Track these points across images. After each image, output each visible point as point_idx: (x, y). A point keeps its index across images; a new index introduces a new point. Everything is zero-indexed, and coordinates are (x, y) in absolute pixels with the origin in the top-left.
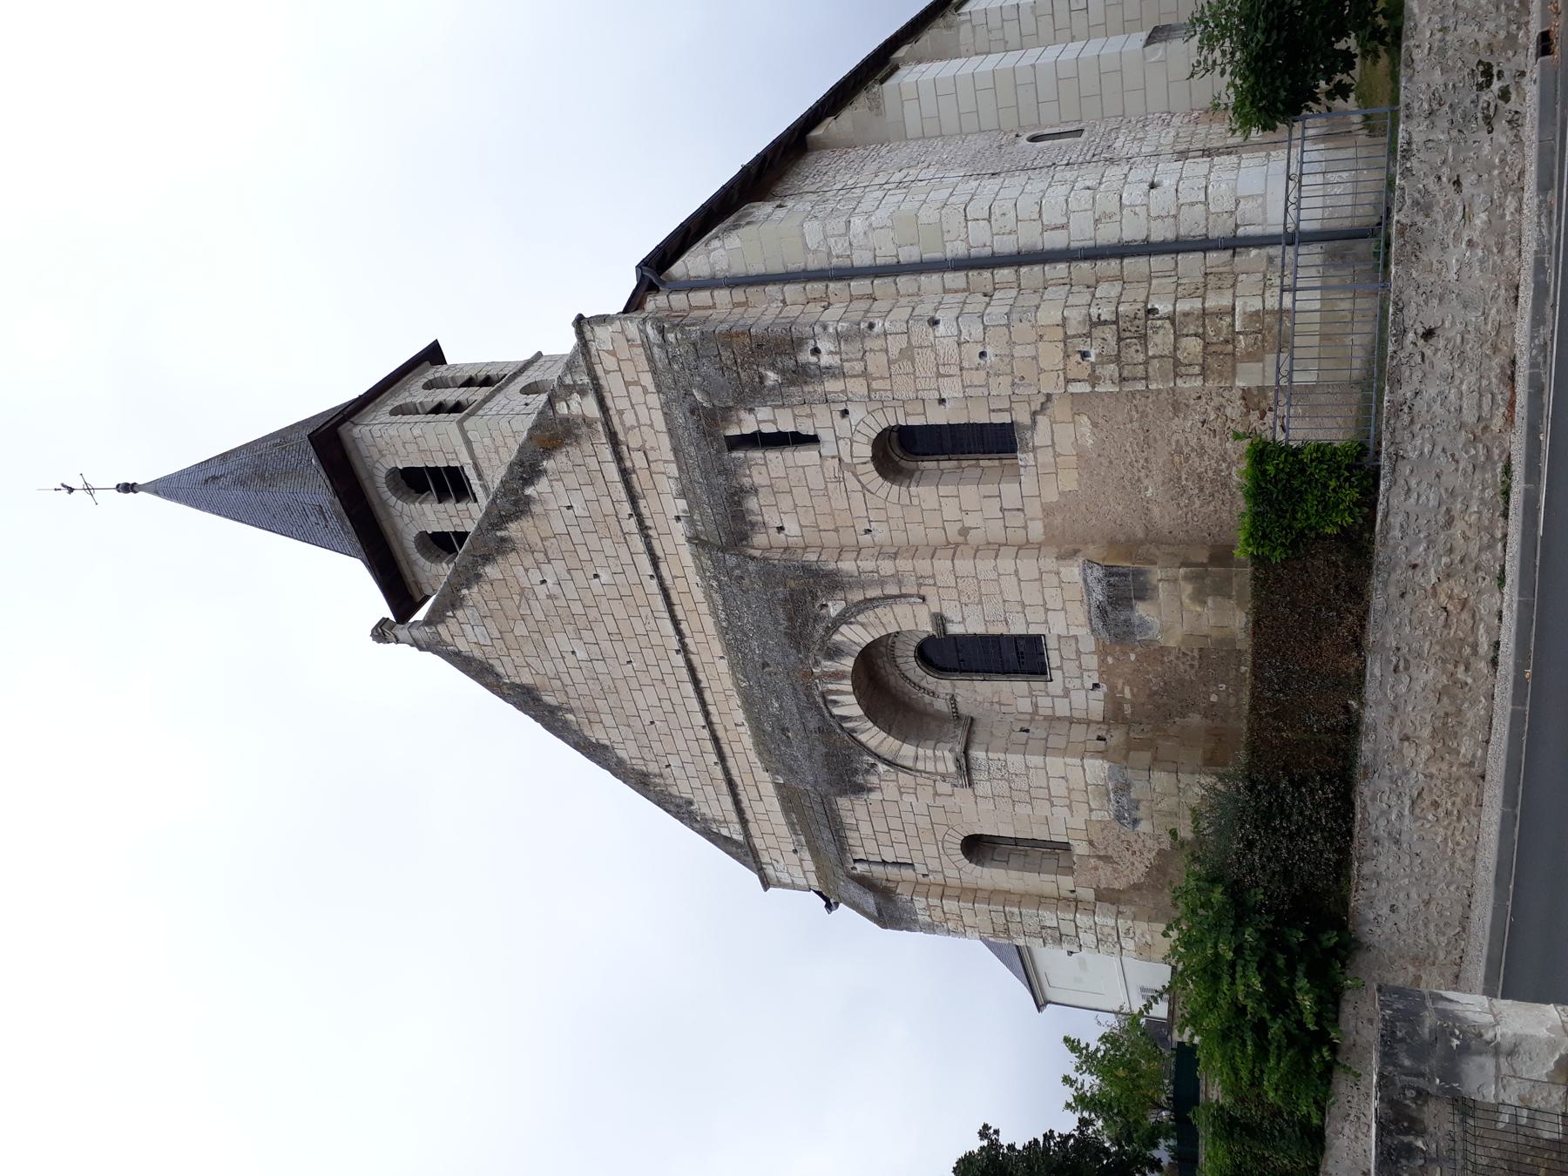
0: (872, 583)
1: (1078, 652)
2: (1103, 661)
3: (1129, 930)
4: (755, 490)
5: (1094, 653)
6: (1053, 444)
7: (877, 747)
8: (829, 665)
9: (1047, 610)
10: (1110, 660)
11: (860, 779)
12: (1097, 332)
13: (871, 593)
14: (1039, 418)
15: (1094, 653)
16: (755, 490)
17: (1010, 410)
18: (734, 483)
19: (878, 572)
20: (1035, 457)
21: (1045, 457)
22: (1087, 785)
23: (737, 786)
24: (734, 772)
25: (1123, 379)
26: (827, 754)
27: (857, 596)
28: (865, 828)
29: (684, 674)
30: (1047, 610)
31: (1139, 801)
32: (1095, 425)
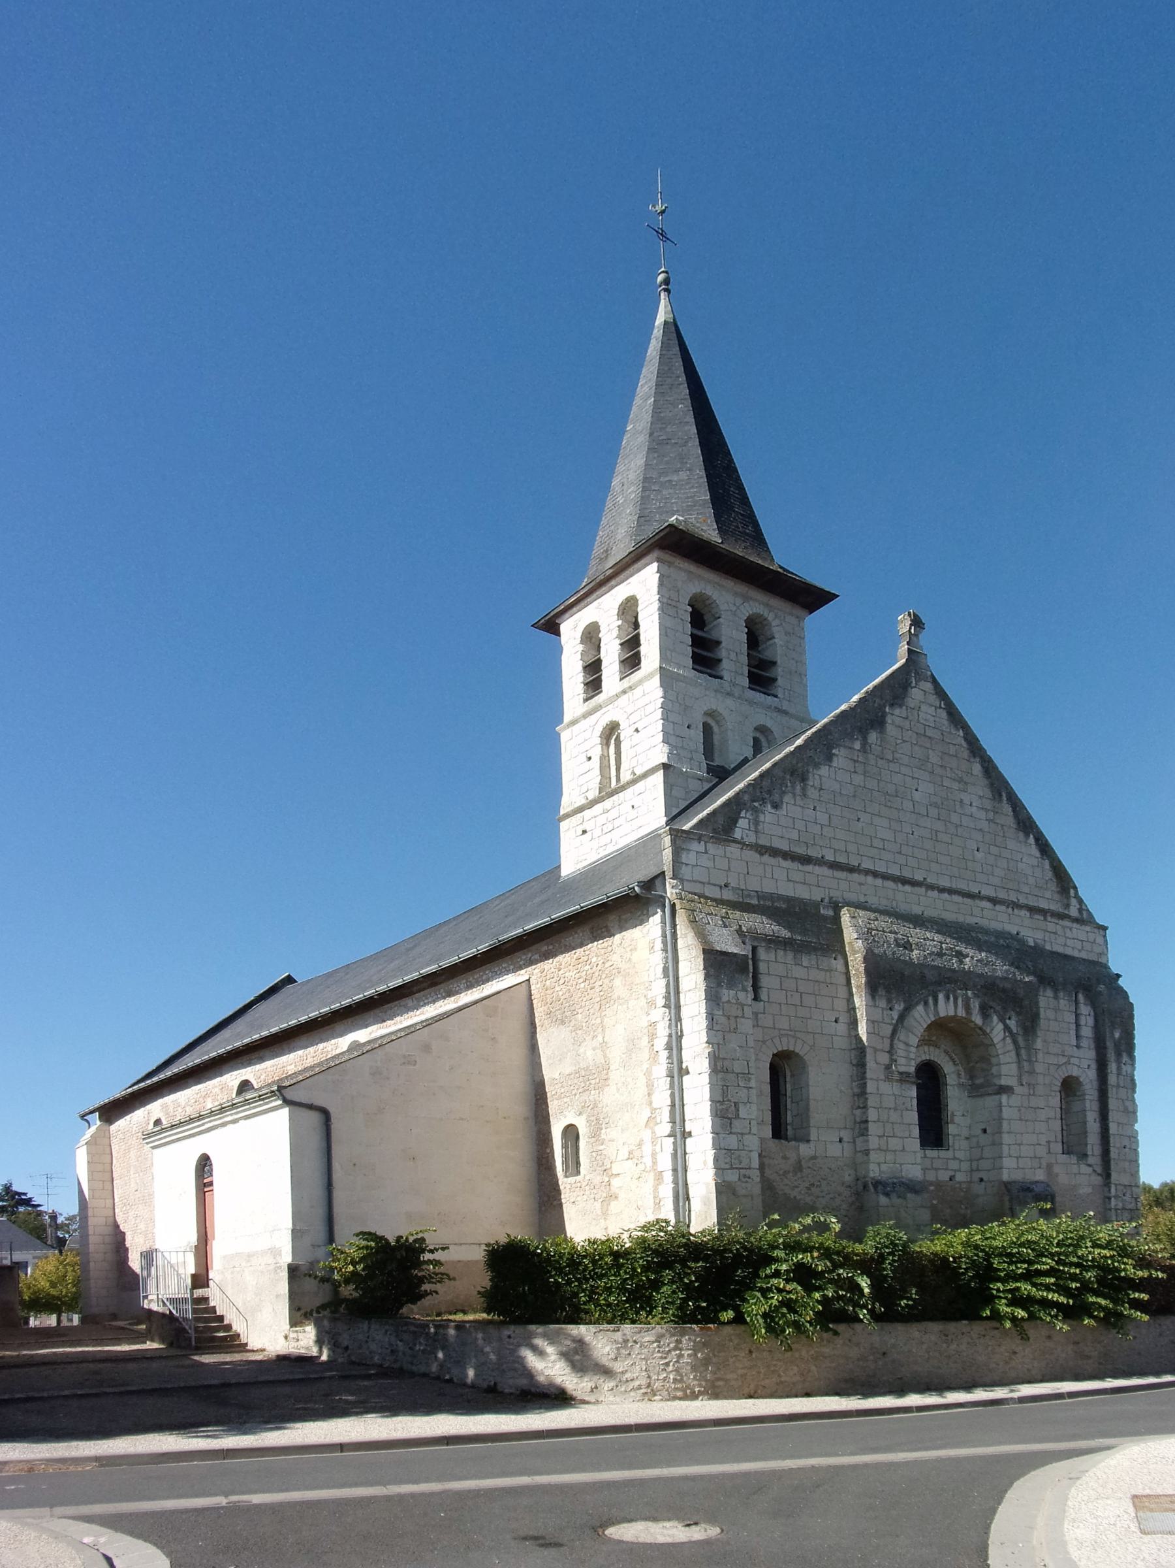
0: (1029, 1055)
1: (937, 1169)
2: (931, 1184)
3: (749, 1178)
4: (1056, 997)
5: (937, 1179)
6: (1080, 1174)
7: (913, 1016)
8: (975, 1005)
9: (1017, 1158)
10: (932, 1188)
11: (881, 992)
12: (1133, 1200)
13: (1023, 1052)
14: (1091, 1169)
15: (937, 1179)
16: (1056, 997)
17: (1093, 1155)
18: (1060, 987)
19: (1036, 1061)
20: (1074, 1164)
21: (1075, 1169)
22: (901, 1164)
23: (802, 864)
24: (818, 870)
25: (1116, 1210)
26: (903, 974)
27: (1020, 1040)
28: (799, 972)
29: (907, 874)
30: (1017, 1158)
31: (905, 1198)
32: (1088, 1194)
